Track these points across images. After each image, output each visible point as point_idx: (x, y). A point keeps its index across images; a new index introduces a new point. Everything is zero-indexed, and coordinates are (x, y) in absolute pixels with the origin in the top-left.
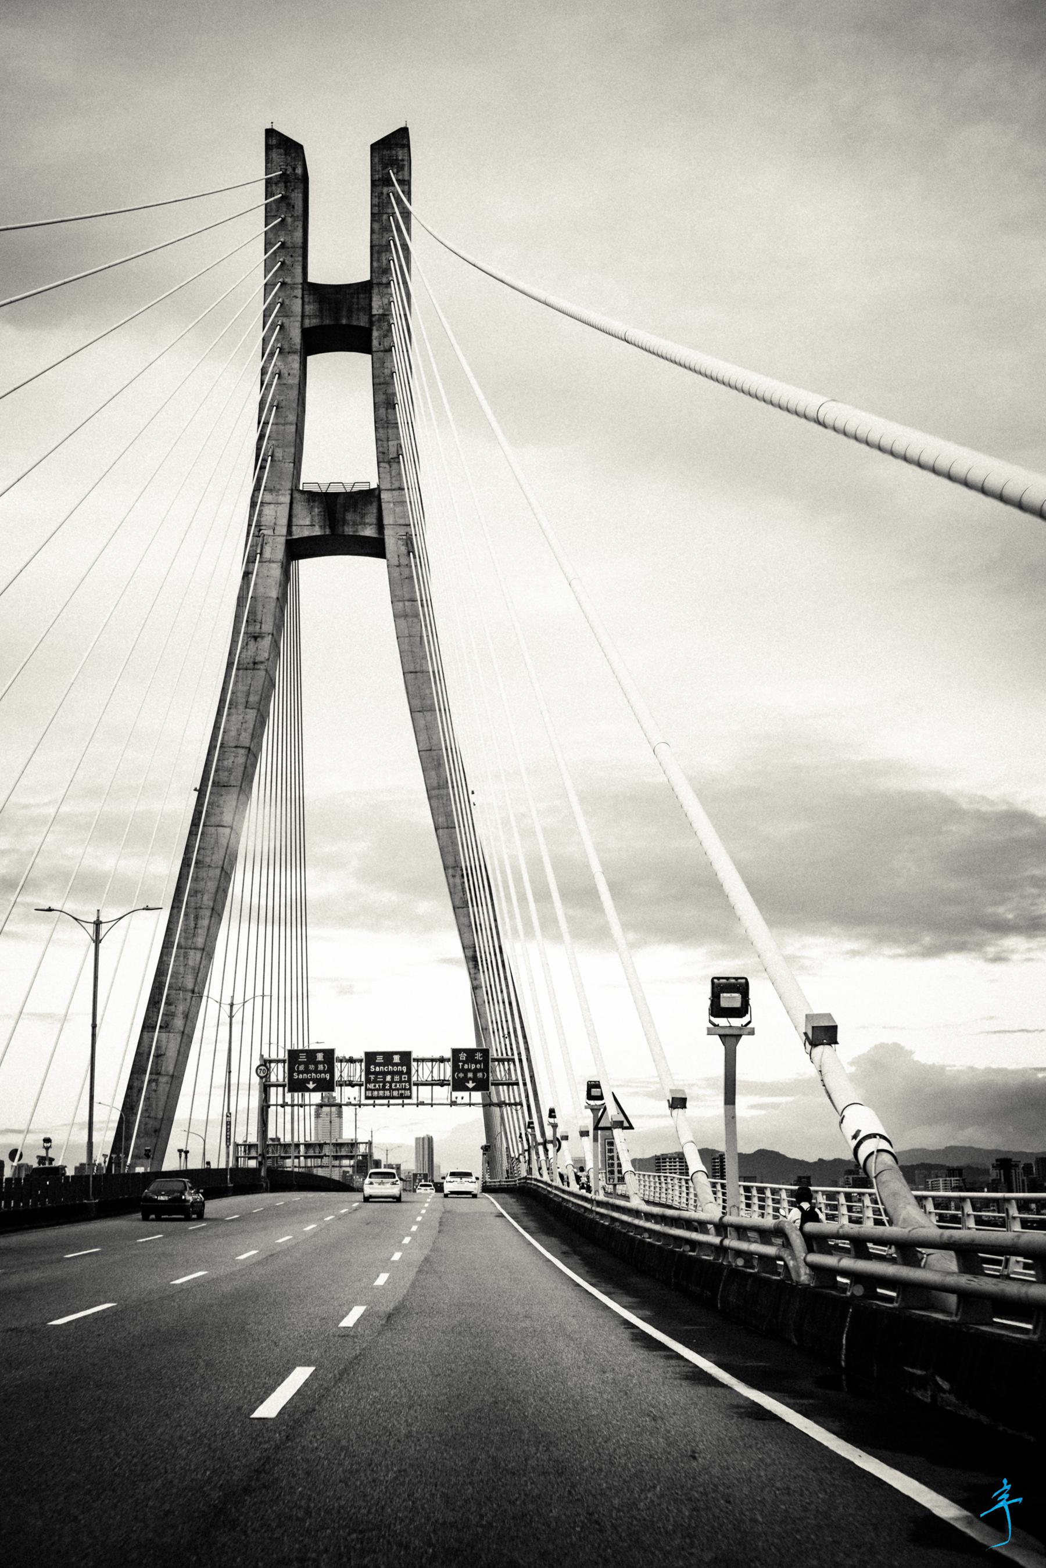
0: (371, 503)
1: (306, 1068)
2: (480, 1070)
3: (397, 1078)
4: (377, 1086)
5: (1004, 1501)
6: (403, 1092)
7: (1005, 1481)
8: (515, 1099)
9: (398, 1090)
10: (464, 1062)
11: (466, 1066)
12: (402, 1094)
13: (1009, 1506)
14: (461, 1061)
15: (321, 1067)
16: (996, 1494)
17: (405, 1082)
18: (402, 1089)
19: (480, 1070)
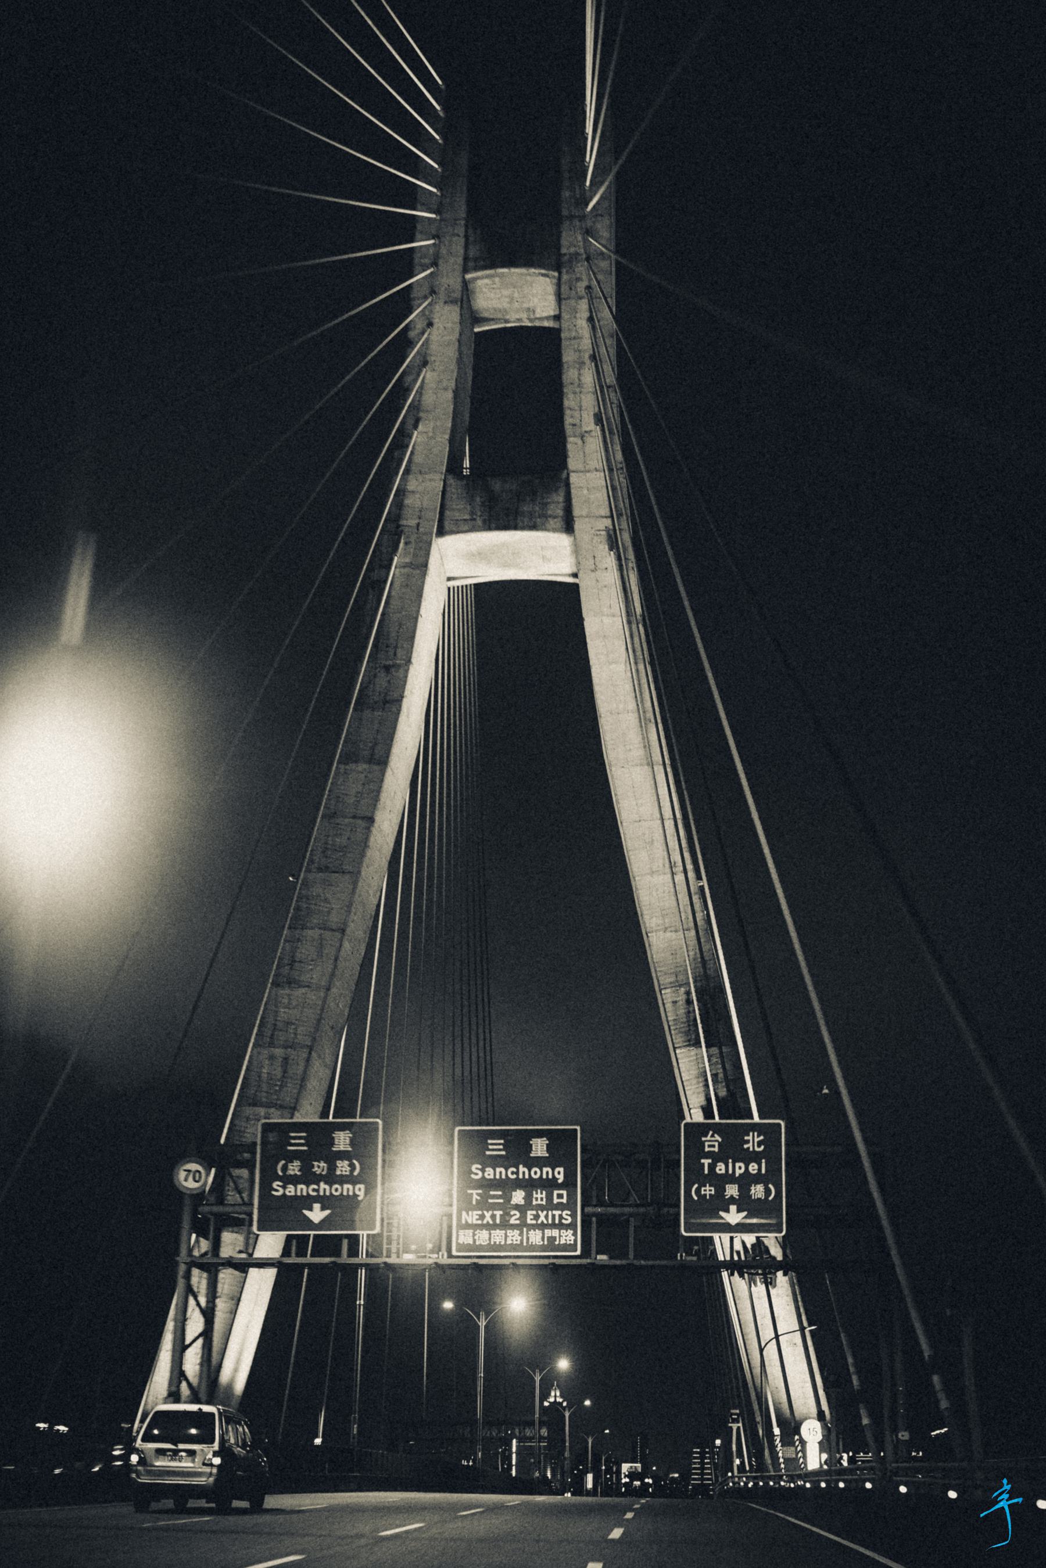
0: (556, 490)
1: (307, 1168)
2: (758, 1179)
3: (539, 1197)
4: (488, 1219)
5: (1004, 1501)
6: (555, 1233)
7: (1005, 1481)
8: (500, 1144)
9: (543, 1227)
10: (716, 1158)
11: (720, 1169)
12: (552, 1239)
13: (1009, 1506)
14: (708, 1155)
15: (343, 1167)
16: (996, 1494)
17: (561, 1207)
18: (553, 1226)
19: (758, 1179)
